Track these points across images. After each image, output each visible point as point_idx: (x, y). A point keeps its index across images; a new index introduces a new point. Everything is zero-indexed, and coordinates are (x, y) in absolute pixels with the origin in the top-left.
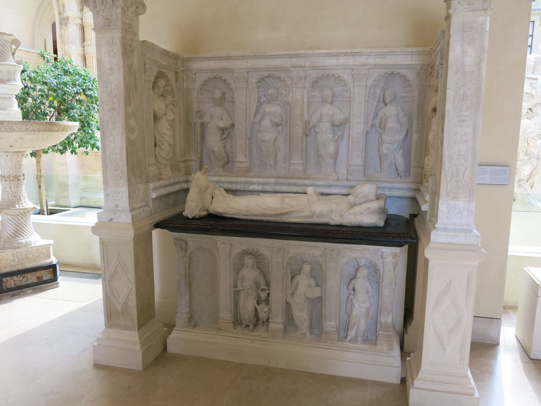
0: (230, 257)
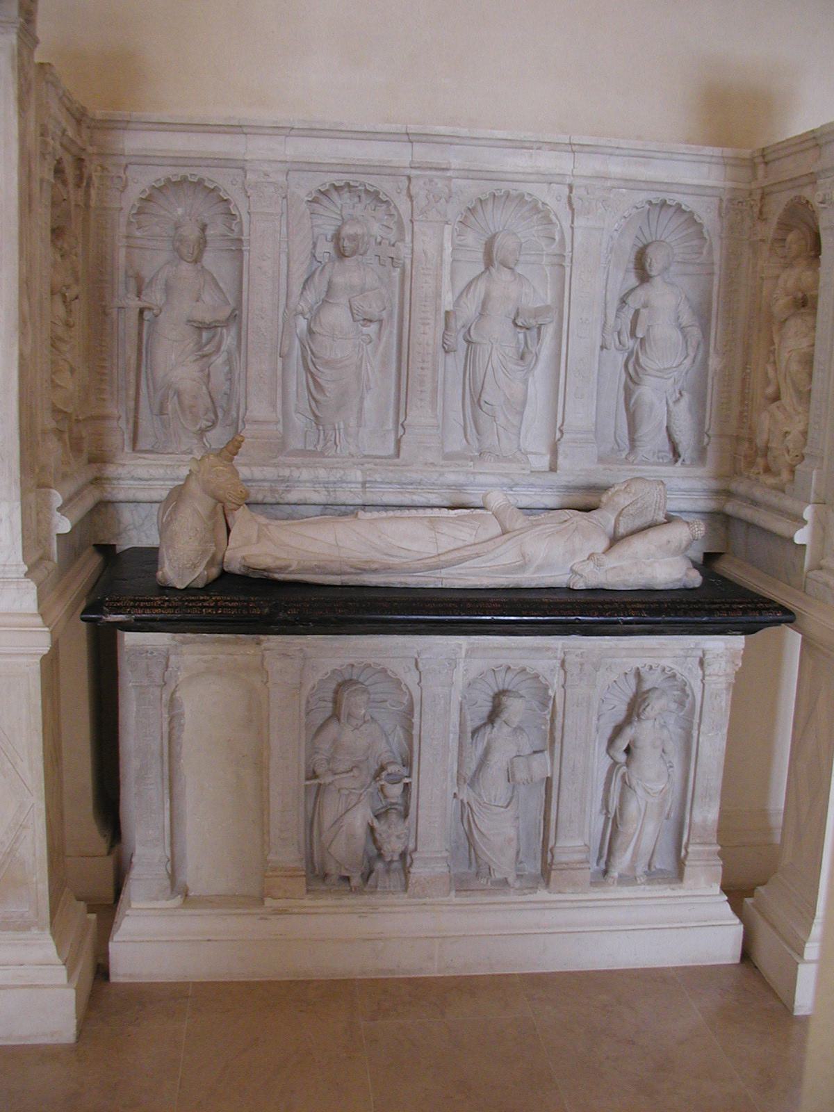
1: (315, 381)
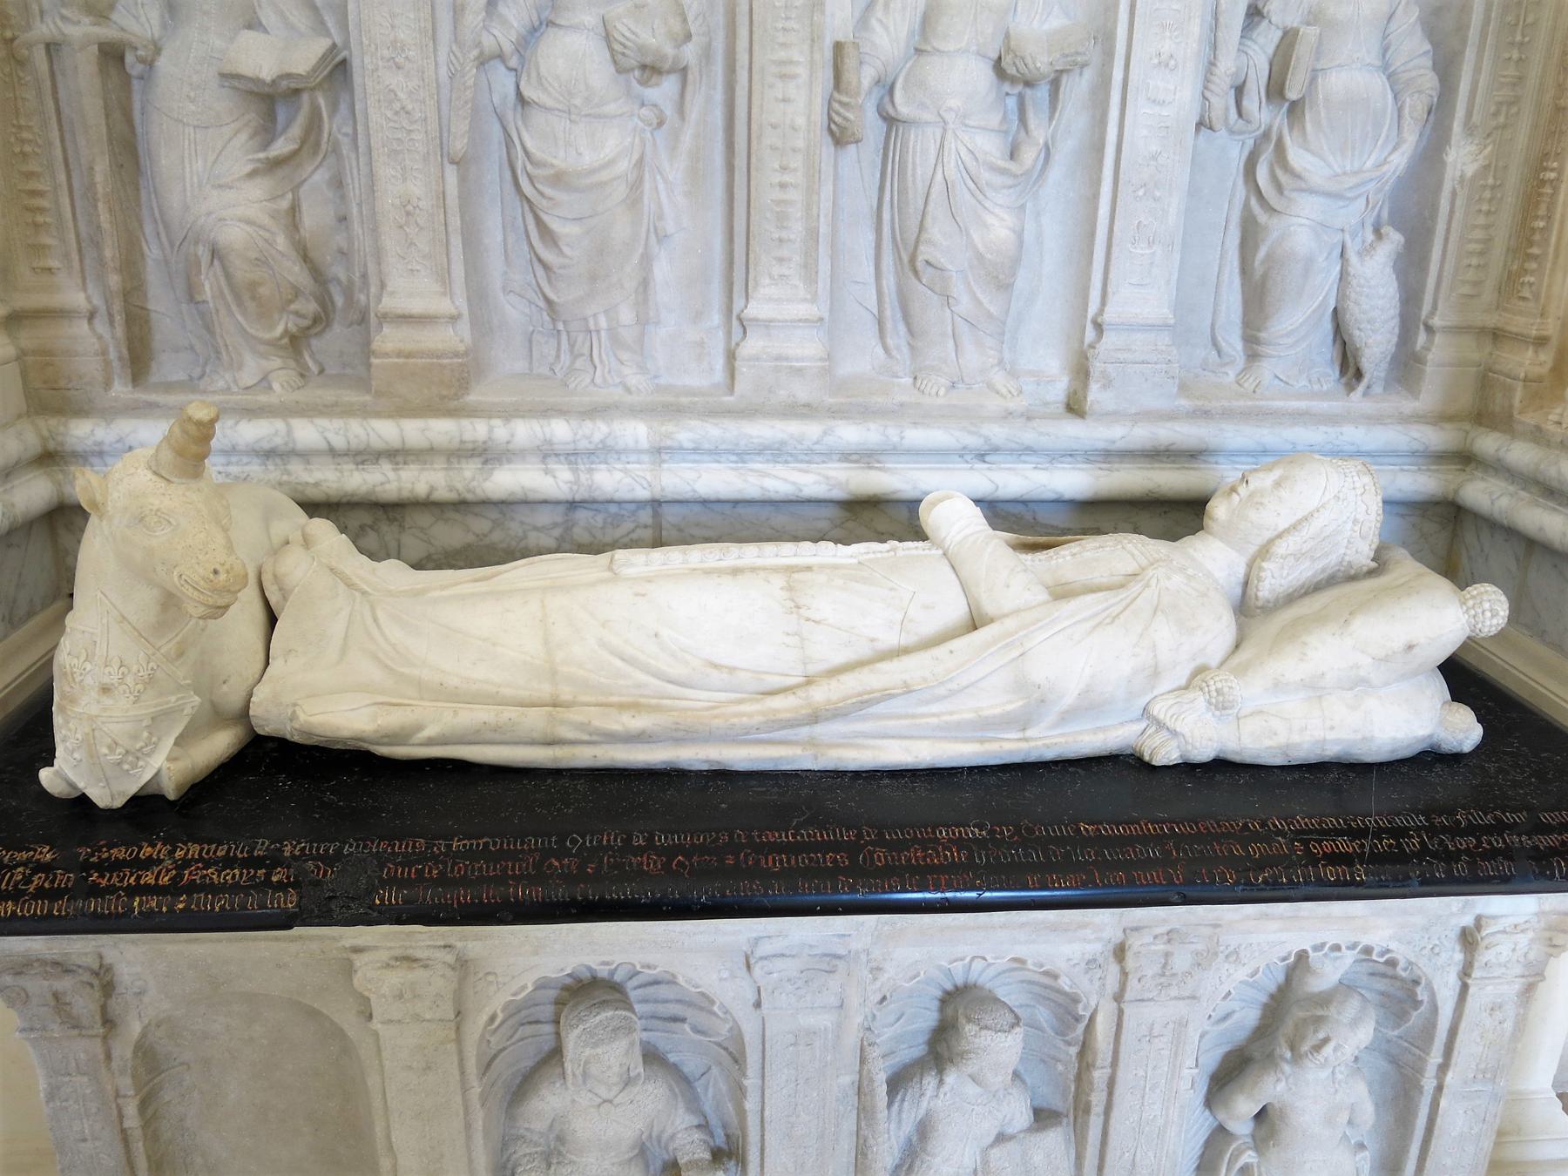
0: (459, 1040)
1: (539, 222)
